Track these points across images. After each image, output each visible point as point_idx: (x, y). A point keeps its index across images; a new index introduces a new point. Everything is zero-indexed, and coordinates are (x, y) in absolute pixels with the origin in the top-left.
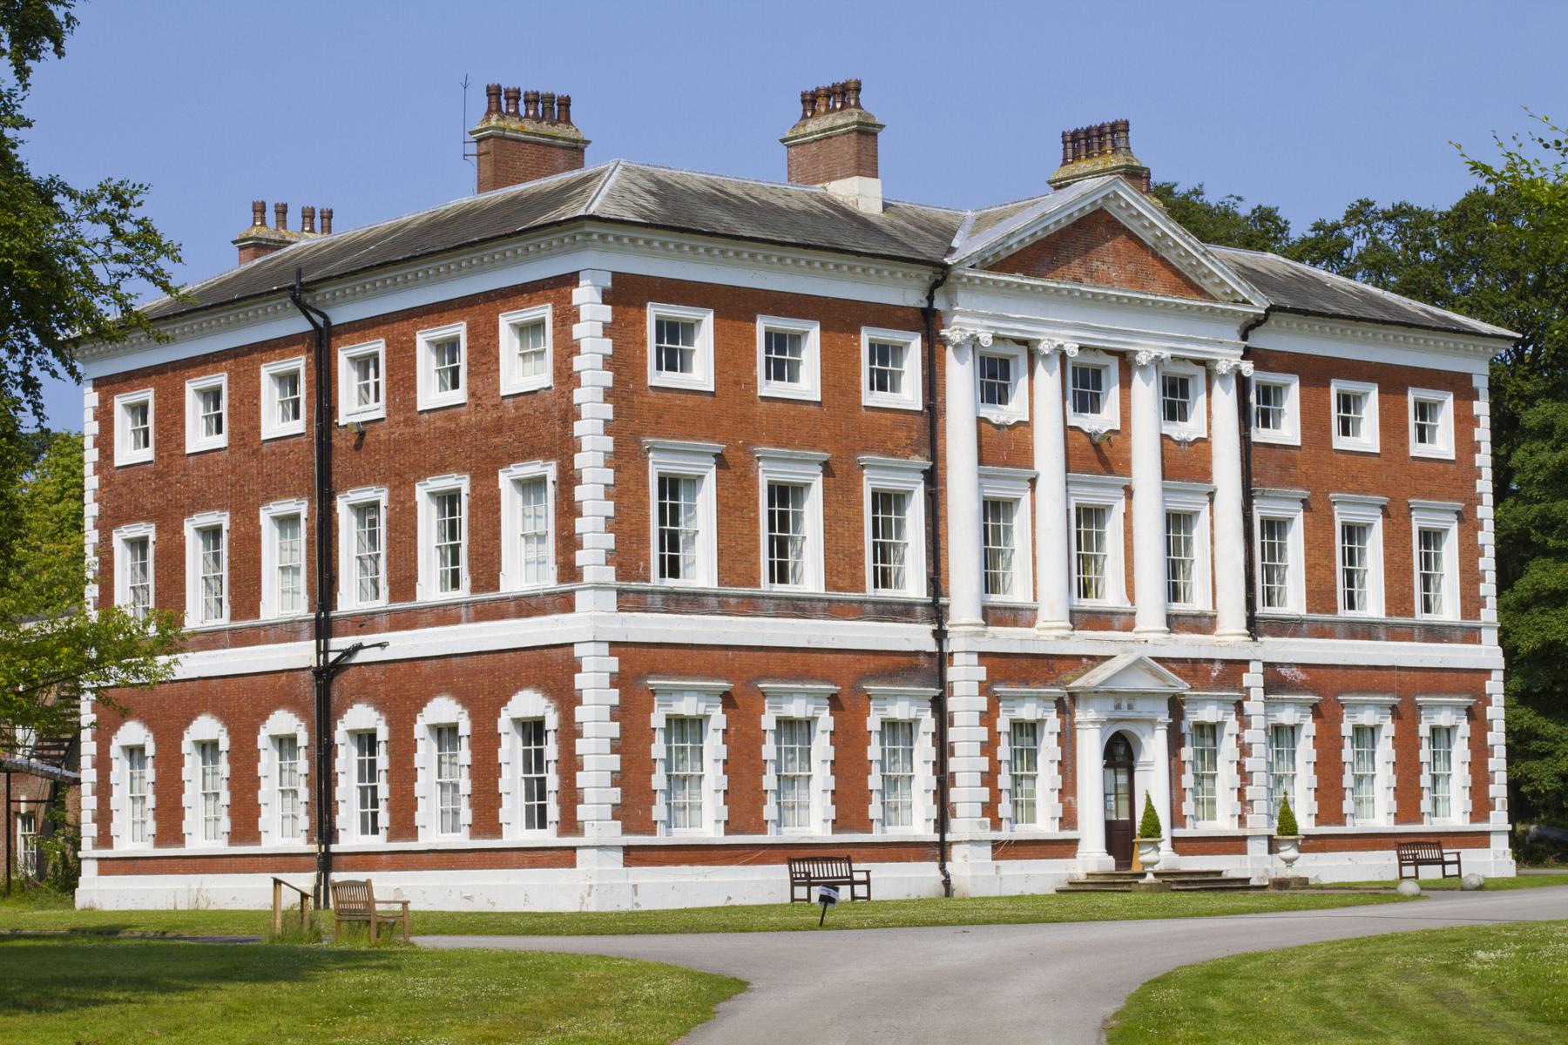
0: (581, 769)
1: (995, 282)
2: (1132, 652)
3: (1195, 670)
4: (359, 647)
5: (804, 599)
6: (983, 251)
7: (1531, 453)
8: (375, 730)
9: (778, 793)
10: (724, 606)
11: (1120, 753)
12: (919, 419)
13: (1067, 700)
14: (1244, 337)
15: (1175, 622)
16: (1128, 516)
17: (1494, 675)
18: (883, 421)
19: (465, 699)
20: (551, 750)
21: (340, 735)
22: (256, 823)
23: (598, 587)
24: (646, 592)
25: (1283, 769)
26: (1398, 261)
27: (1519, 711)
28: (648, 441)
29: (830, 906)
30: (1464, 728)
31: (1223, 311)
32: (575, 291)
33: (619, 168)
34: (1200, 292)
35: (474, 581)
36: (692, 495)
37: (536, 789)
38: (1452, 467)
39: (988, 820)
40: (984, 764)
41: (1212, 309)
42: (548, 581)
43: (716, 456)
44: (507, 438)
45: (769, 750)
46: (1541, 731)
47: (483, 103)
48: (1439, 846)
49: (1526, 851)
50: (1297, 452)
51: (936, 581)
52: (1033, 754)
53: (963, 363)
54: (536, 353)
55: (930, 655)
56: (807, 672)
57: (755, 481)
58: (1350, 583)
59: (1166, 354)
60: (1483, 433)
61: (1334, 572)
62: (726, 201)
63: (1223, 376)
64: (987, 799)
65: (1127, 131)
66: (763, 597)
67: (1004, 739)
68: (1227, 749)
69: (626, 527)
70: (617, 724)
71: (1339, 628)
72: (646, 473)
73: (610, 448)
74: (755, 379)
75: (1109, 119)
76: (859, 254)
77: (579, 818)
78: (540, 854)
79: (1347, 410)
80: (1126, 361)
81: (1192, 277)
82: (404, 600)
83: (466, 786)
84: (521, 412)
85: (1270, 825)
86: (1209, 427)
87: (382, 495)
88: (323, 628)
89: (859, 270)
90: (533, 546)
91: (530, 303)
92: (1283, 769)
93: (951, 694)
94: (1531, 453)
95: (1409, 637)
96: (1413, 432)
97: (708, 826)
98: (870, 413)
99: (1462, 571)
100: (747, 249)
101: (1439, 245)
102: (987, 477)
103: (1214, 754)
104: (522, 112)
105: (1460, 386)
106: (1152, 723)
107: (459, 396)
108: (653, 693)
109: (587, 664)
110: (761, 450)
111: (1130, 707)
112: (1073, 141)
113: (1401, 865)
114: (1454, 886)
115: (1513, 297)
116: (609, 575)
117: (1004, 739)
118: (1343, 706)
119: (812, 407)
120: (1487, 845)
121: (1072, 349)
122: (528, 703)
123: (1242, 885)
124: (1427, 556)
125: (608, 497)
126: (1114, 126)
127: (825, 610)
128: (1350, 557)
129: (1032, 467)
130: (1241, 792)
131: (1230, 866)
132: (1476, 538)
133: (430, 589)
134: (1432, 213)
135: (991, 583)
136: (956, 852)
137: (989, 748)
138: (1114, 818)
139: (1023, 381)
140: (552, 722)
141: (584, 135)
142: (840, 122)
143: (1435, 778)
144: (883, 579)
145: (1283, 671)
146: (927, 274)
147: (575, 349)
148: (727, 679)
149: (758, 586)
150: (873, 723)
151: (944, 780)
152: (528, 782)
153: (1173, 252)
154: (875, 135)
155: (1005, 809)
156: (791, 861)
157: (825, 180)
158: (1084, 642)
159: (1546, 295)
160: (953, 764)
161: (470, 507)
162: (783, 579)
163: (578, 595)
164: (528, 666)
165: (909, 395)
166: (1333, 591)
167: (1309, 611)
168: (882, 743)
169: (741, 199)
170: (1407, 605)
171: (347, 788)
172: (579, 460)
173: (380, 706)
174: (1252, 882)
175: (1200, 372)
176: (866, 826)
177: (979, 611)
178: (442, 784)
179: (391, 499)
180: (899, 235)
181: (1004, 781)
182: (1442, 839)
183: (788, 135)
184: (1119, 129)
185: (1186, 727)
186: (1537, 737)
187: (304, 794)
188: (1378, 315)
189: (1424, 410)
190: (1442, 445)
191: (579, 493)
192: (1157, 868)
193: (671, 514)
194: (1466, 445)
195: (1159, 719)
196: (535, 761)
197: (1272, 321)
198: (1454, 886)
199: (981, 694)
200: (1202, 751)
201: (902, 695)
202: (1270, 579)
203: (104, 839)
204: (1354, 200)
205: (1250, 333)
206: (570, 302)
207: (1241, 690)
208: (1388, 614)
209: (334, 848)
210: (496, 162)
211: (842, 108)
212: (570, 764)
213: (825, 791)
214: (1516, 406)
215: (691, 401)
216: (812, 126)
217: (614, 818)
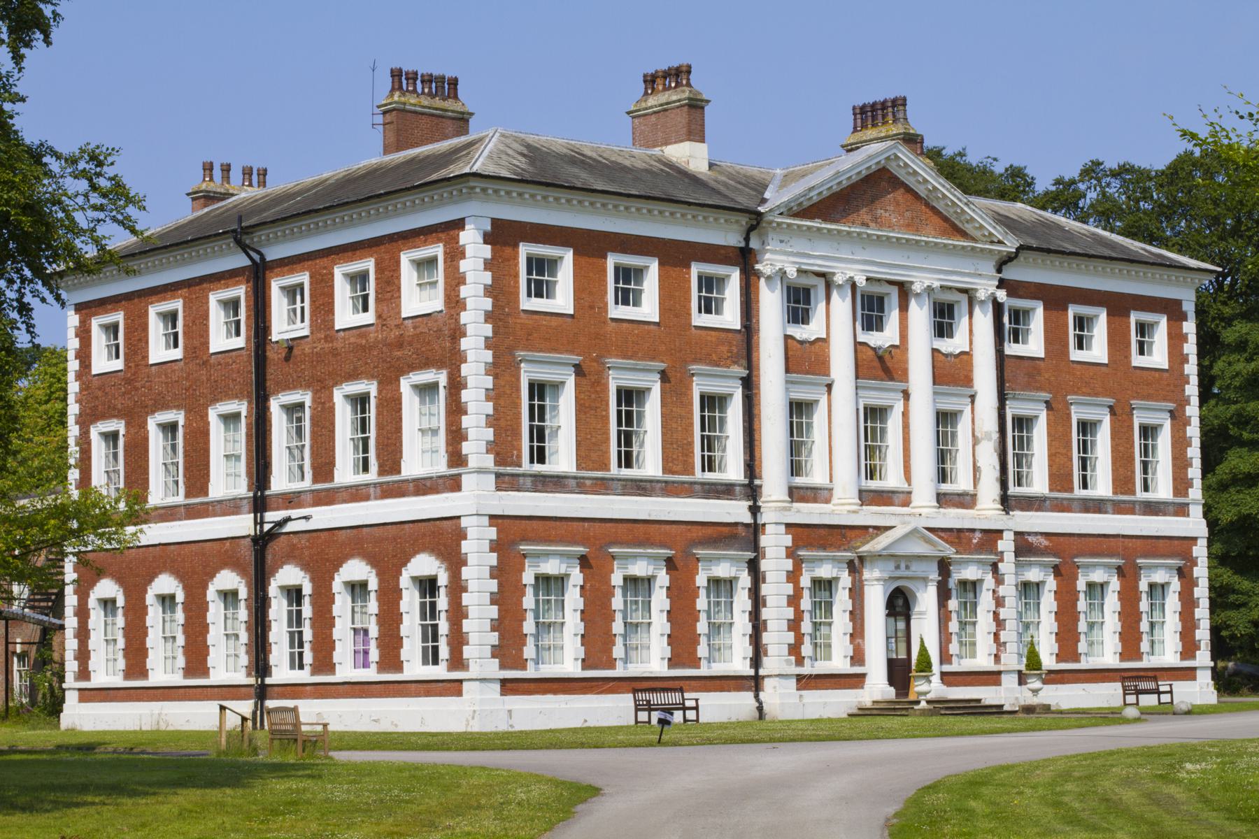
1: (799, 226)
2: (909, 523)
4: (288, 519)
5: (646, 481)
6: (789, 201)
7: (1230, 364)
8: (301, 586)
9: (625, 636)
10: (581, 486)
11: (900, 605)
12: (739, 336)
13: (856, 562)
14: (999, 271)
15: (943, 499)
16: (905, 414)
18: (709, 338)
19: (373, 561)
20: (442, 602)
21: (273, 590)
22: (205, 660)
23: (481, 471)
24: (518, 475)
25: (1030, 617)
26: (1122, 209)
28: (521, 354)
30: (1176, 585)
31: (982, 250)
32: (462, 234)
33: (497, 135)
34: (964, 234)
35: (380, 466)
36: (556, 398)
37: (430, 634)
38: (1166, 375)
39: (793, 658)
40: (790, 613)
41: (973, 248)
42: (440, 466)
43: (575, 366)
44: (407, 351)
45: (617, 602)
46: (1237, 587)
48: (1155, 679)
51: (752, 466)
52: (829, 605)
55: (747, 525)
56: (648, 539)
58: (1084, 468)
59: (936, 284)
60: (1191, 348)
61: (1071, 460)
62: (583, 162)
64: (792, 641)
65: (905, 105)
66: (613, 479)
67: (806, 594)
68: (985, 601)
71: (1075, 505)
73: (490, 359)
75: (891, 96)
76: (689, 204)
77: (465, 657)
78: (434, 685)
79: (1081, 329)
80: (904, 290)
82: (325, 481)
83: (374, 631)
84: (418, 331)
88: (260, 504)
90: (428, 438)
91: (425, 243)
92: (1030, 617)
93: (764, 557)
94: (1230, 364)
97: (569, 663)
98: (699, 332)
99: (1174, 458)
100: (600, 200)
101: (1155, 197)
102: (792, 382)
103: (975, 605)
105: (1172, 310)
106: (925, 580)
107: (369, 318)
108: (525, 556)
109: (471, 533)
110: (611, 361)
111: (907, 567)
112: (861, 114)
113: (1125, 694)
114: (1167, 711)
115: (1215, 238)
116: (489, 461)
117: (806, 594)
118: (1078, 567)
119: (652, 327)
120: (1194, 678)
121: (861, 280)
122: (424, 564)
123: (998, 710)
124: (1146, 446)
125: (488, 399)
127: (662, 489)
128: (1084, 447)
129: (828, 375)
130: (996, 635)
131: (987, 695)
132: (1185, 432)
133: (345, 473)
134: (1150, 171)
135: (796, 468)
136: (767, 683)
137: (794, 600)
138: (894, 656)
139: (822, 306)
140: (443, 580)
141: (469, 108)
142: (674, 98)
143: (1152, 625)
144: (709, 465)
145: (1030, 539)
146: (744, 220)
147: (461, 280)
149: (609, 470)
150: (701, 580)
151: (758, 626)
152: (291, 634)
153: (942, 203)
154: (703, 108)
155: (807, 649)
156: (635, 691)
157: (661, 145)
158: (870, 516)
161: (377, 407)
162: (629, 465)
165: (730, 317)
166: (1071, 475)
167: (1051, 490)
169: (594, 160)
170: (1130, 486)
171: (279, 633)
172: (465, 369)
173: (306, 567)
174: (1005, 708)
175: (964, 299)
176: (695, 663)
179: (314, 400)
180: (722, 189)
181: (806, 627)
182: (1158, 673)
183: (633, 108)
185: (952, 583)
186: (1234, 591)
187: (244, 637)
188: (1107, 252)
189: (1143, 329)
190: (1158, 357)
191: (465, 395)
193: (538, 413)
194: (1177, 357)
195: (931, 577)
196: (429, 611)
197: (1021, 257)
198: (1167, 711)
199: (788, 557)
200: (965, 603)
201: (725, 558)
202: (1019, 465)
203: (84, 674)
204: (1087, 161)
205: (1004, 267)
206: (458, 242)
207: (996, 554)
208: (1115, 493)
209: (268, 681)
210: (398, 130)
212: (458, 613)
213: (662, 635)
214: (1217, 326)
215: (555, 322)
216: (652, 101)
217: (493, 656)
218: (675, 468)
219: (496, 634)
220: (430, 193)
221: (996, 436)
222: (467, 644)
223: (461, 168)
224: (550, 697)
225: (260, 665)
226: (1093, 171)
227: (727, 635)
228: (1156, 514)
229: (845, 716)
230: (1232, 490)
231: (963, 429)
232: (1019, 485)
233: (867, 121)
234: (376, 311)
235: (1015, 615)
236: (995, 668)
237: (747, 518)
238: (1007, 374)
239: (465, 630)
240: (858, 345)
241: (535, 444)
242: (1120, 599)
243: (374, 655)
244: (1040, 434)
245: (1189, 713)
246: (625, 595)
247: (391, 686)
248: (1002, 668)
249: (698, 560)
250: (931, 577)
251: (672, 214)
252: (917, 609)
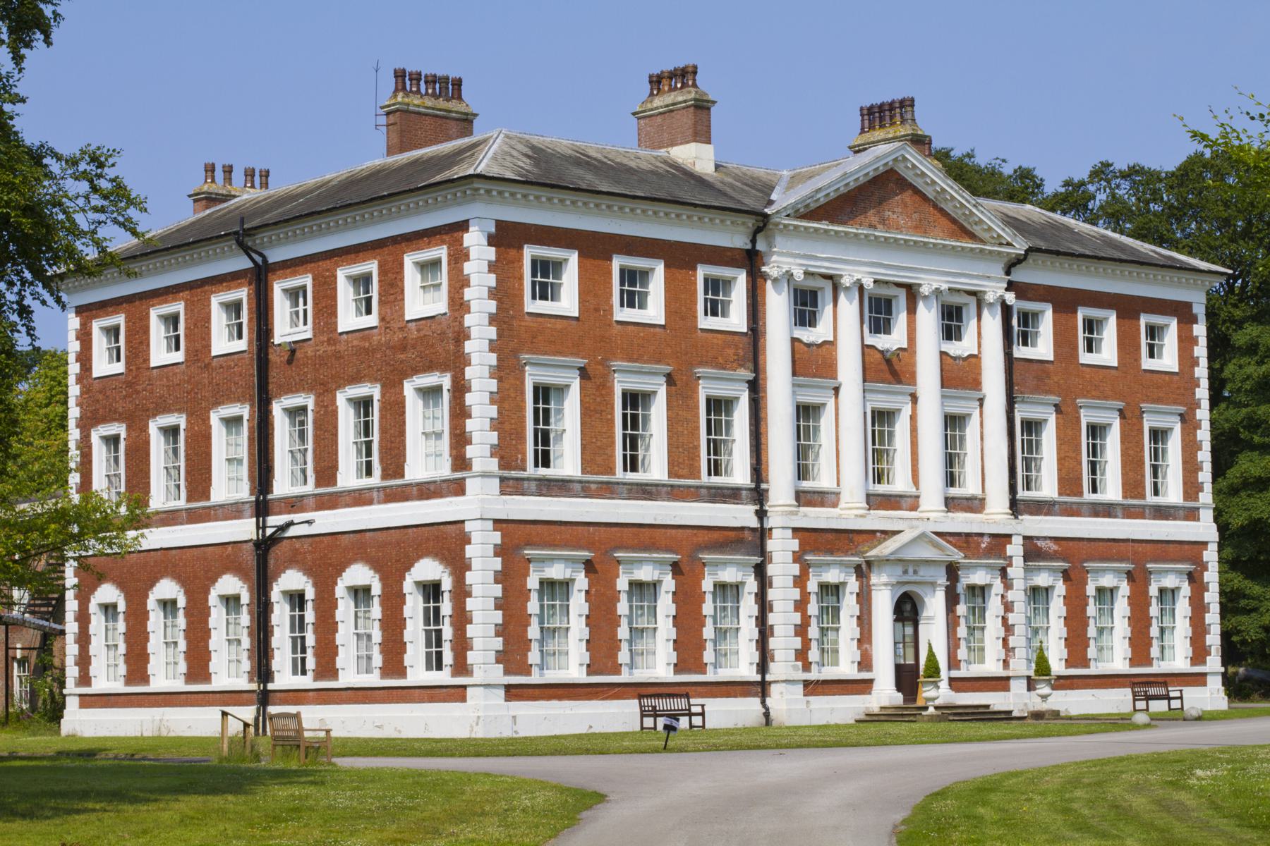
1: (806, 228)
2: (917, 527)
4: (291, 524)
5: (652, 485)
6: (796, 203)
7: (1240, 367)
8: (304, 590)
9: (630, 642)
10: (586, 490)
11: (907, 610)
12: (745, 339)
13: (864, 566)
14: (1008, 273)
15: (951, 504)
16: (913, 418)
18: (715, 341)
19: (376, 565)
20: (446, 607)
21: (275, 595)
22: (207, 666)
23: (485, 475)
24: (523, 479)
25: (1039, 622)
26: (1132, 211)
28: (525, 357)
30: (1186, 589)
31: (991, 252)
32: (466, 236)
33: (502, 136)
34: (972, 236)
35: (384, 470)
36: (561, 401)
37: (434, 639)
38: (1176, 378)
39: (800, 664)
40: (797, 618)
41: (982, 250)
42: (444, 470)
43: (580, 369)
44: (411, 354)
45: (623, 607)
46: (1247, 592)
48: (1165, 685)
51: (758, 470)
52: (837, 610)
55: (753, 530)
56: (654, 544)
58: (1094, 472)
59: (944, 287)
60: (1201, 351)
61: (1080, 463)
62: (588, 163)
64: (799, 646)
65: (912, 106)
66: (618, 483)
67: (813, 599)
68: (994, 606)
71: (1084, 509)
73: (494, 362)
75: (898, 96)
76: (695, 205)
77: (469, 662)
78: (437, 691)
79: (1091, 332)
80: (912, 292)
82: (327, 485)
83: (377, 636)
84: (422, 334)
85: (1029, 668)
88: (262, 508)
90: (432, 442)
91: (429, 245)
92: (1039, 622)
93: (771, 562)
94: (1240, 367)
97: (573, 668)
98: (705, 334)
99: (1185, 462)
100: (605, 201)
101: (1165, 198)
102: (799, 386)
103: (983, 610)
105: (1183, 312)
106: (933, 585)
107: (372, 320)
108: (529, 561)
109: (475, 538)
110: (616, 364)
111: (915, 572)
112: (869, 114)
113: (1135, 700)
114: (1177, 717)
115: (1225, 240)
116: (493, 465)
117: (813, 599)
118: (1088, 572)
119: (658, 330)
120: (1205, 684)
121: (868, 283)
122: (428, 569)
123: (1006, 716)
124: (1156, 450)
125: (492, 402)
127: (668, 493)
128: (1094, 451)
129: (836, 378)
130: (1005, 641)
131: (996, 701)
132: (1195, 436)
133: (348, 477)
134: (1160, 173)
135: (802, 472)
136: (774, 689)
137: (801, 605)
138: (902, 662)
139: (829, 309)
140: (447, 585)
141: (473, 109)
142: (680, 99)
143: (1162, 630)
144: (715, 468)
145: (1039, 543)
146: (751, 222)
147: (465, 282)
149: (614, 474)
150: (707, 585)
151: (765, 632)
152: (294, 639)
153: (950, 204)
154: (709, 109)
155: (814, 655)
156: (640, 697)
157: (667, 147)
158: (878, 520)
161: (381, 411)
162: (634, 468)
164: (428, 539)
165: (736, 320)
166: (1080, 479)
167: (1060, 494)
169: (600, 161)
170: (1140, 490)
171: (281, 638)
172: (469, 372)
173: (308, 572)
174: (1014, 714)
175: (972, 301)
176: (702, 668)
179: (317, 404)
180: (728, 190)
181: (813, 632)
182: (1168, 679)
183: (638, 109)
184: (906, 104)
185: (960, 588)
186: (1245, 596)
187: (246, 642)
188: (1117, 255)
189: (1153, 331)
190: (1168, 360)
191: (469, 399)
193: (543, 416)
194: (1187, 360)
195: (939, 582)
196: (433, 616)
197: (1030, 260)
198: (1177, 717)
199: (795, 561)
200: (974, 608)
201: (731, 562)
202: (1028, 469)
203: (84, 679)
204: (1097, 162)
205: (1013, 270)
206: (462, 244)
207: (1005, 558)
208: (1125, 497)
209: (270, 686)
210: (402, 131)
212: (462, 618)
213: (668, 640)
214: (1228, 328)
215: (559, 325)
216: (658, 102)
217: (498, 662)
218: (681, 472)
219: (501, 639)
220: (434, 195)
222: (472, 649)
223: (465, 169)
224: (555, 703)
225: (263, 671)
226: (1103, 172)
227: (733, 641)
228: (1167, 518)
229: (852, 722)
230: (1243, 494)
232: (1028, 489)
233: (874, 122)
234: (380, 314)
235: (1024, 621)
236: (1003, 673)
237: (753, 522)
238: (1016, 377)
239: (469, 635)
240: (866, 348)
241: (540, 448)
242: (1130, 604)
244: (1049, 438)
245: (1199, 719)
246: (630, 600)
247: (395, 692)
248: (1010, 674)
249: (704, 564)
250: (939, 582)
251: (678, 216)
252: (925, 614)
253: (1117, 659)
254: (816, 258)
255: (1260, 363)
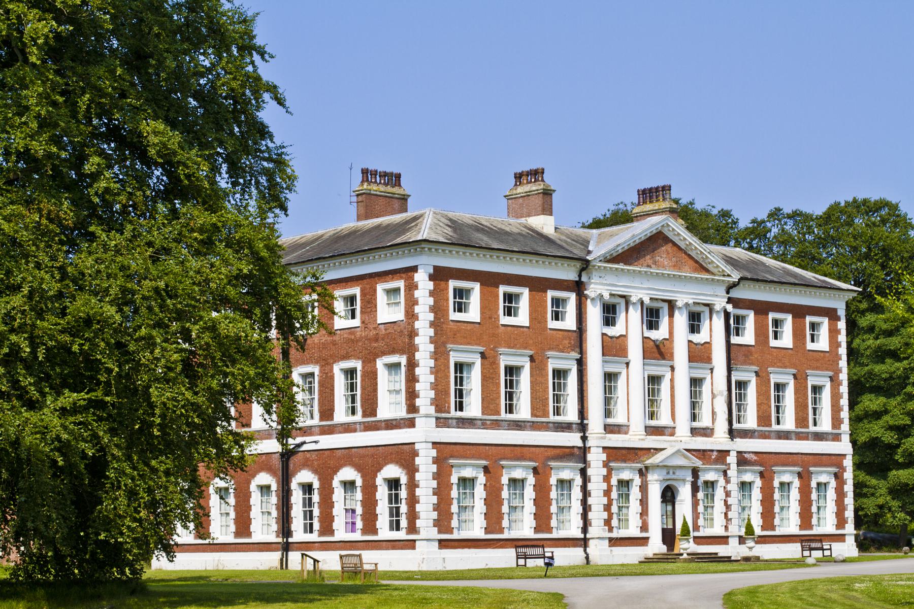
0: (419, 503)
1: (610, 268)
2: (675, 446)
3: (704, 455)
4: (304, 443)
5: (521, 421)
6: (605, 253)
7: (863, 341)
8: (312, 483)
9: (459, 514)
10: (484, 425)
11: (669, 496)
12: (575, 334)
13: (644, 469)
14: (728, 293)
15: (694, 432)
16: (672, 380)
17: (847, 456)
18: (558, 336)
19: (359, 468)
20: (403, 493)
21: (294, 485)
22: (249, 528)
23: (427, 416)
24: (448, 418)
25: (746, 503)
26: (795, 240)
27: (858, 473)
28: (450, 346)
29: (550, 568)
30: (833, 483)
31: (718, 280)
32: (416, 275)
33: (432, 213)
34: (707, 271)
35: (363, 412)
36: (469, 372)
37: (395, 513)
38: (827, 355)
39: (607, 528)
40: (605, 500)
41: (713, 280)
42: (401, 412)
43: (481, 353)
44: (381, 344)
45: (505, 494)
46: (868, 483)
47: (360, 177)
48: (821, 541)
49: (863, 545)
50: (753, 348)
51: (582, 413)
52: (628, 496)
53: (595, 307)
54: (395, 303)
55: (579, 448)
56: (523, 456)
57: (498, 365)
58: (778, 412)
59: (691, 302)
60: (842, 338)
61: (770, 407)
62: (483, 229)
63: (718, 312)
64: (606, 517)
65: (670, 190)
66: (502, 421)
67: (614, 489)
68: (719, 494)
69: (440, 387)
70: (436, 481)
71: (773, 435)
72: (449, 361)
73: (433, 350)
74: (499, 316)
75: (661, 184)
76: (547, 256)
77: (417, 526)
78: (397, 543)
79: (777, 327)
80: (671, 305)
81: (703, 264)
82: (328, 420)
83: (359, 510)
84: (388, 332)
85: (740, 530)
86: (711, 337)
87: (316, 369)
89: (547, 263)
90: (393, 396)
91: (392, 279)
92: (746, 503)
93: (589, 467)
94: (863, 341)
95: (806, 438)
96: (808, 338)
97: (476, 529)
98: (552, 332)
99: (832, 406)
100: (495, 254)
101: (816, 232)
102: (606, 362)
103: (713, 496)
104: (378, 181)
105: (831, 314)
106: (684, 480)
107: (356, 322)
108: (452, 466)
109: (421, 453)
110: (501, 350)
111: (674, 473)
112: (643, 194)
113: (803, 550)
114: (829, 560)
115: (854, 260)
116: (432, 410)
117: (614, 489)
118: (774, 473)
119: (525, 329)
120: (844, 541)
121: (647, 300)
122: (392, 471)
123: (728, 559)
124: (815, 398)
125: (432, 373)
126: (664, 188)
127: (531, 426)
128: (778, 399)
129: (627, 357)
130: (726, 514)
131: (721, 550)
132: (839, 390)
133: (341, 415)
134: (812, 215)
135: (608, 413)
136: (591, 542)
137: (607, 493)
138: (665, 527)
139: (623, 314)
140: (404, 480)
141: (407, 192)
142: (534, 188)
143: (819, 508)
144: (557, 412)
145: (746, 455)
146: (579, 265)
147: (416, 302)
148: (486, 460)
149: (500, 415)
150: (553, 481)
151: (586, 508)
152: (305, 512)
153: (695, 252)
154: (551, 194)
155: (614, 522)
156: (516, 547)
157: (526, 217)
158: (652, 442)
159: (871, 260)
160: (590, 501)
161: (362, 376)
162: (511, 412)
163: (417, 420)
164: (391, 453)
165: (569, 322)
166: (770, 416)
167: (758, 426)
168: (458, 489)
169: (489, 228)
170: (806, 423)
171: (297, 512)
172: (418, 356)
173: (315, 471)
174: (733, 558)
175: (707, 310)
176: (550, 530)
177: (602, 427)
178: (346, 509)
179: (321, 371)
180: (564, 245)
181: (614, 509)
182: (822, 538)
183: (508, 194)
184: (666, 189)
185: (700, 482)
186: (866, 486)
187: (275, 513)
188: (792, 280)
189: (814, 326)
190: (823, 343)
191: (418, 371)
192: (689, 551)
193: (460, 381)
194: (834, 344)
195: (688, 479)
196: (394, 499)
197: (741, 285)
198: (829, 560)
199: (604, 466)
200: (707, 495)
201: (567, 467)
202: (739, 410)
204: (772, 208)
205: (731, 290)
207: (726, 465)
208: (797, 427)
209: (290, 540)
210: (366, 206)
211: (535, 182)
212: (413, 500)
213: (531, 513)
214: (856, 316)
215: (469, 327)
216: (520, 190)
217: (434, 526)
218: (538, 414)
219: (436, 512)
220: (397, 250)
221: (726, 393)
222: (419, 518)
223: (415, 235)
224: (466, 550)
225: (285, 529)
226: (776, 214)
227: (568, 514)
228: (822, 440)
229: (637, 562)
230: (865, 421)
231: (706, 388)
232: (739, 423)
233: (646, 199)
234: (361, 319)
235: (737, 502)
236: (725, 534)
237: (580, 444)
238: (732, 355)
239: (417, 510)
240: (645, 339)
241: (458, 400)
242: (800, 492)
243: (359, 524)
244: (751, 392)
245: (844, 561)
246: (509, 490)
247: (370, 543)
248: (729, 534)
249: (551, 468)
250: (688, 479)
251: (537, 261)
252: (679, 498)
253: (790, 523)
254: (617, 286)
255: (876, 338)
